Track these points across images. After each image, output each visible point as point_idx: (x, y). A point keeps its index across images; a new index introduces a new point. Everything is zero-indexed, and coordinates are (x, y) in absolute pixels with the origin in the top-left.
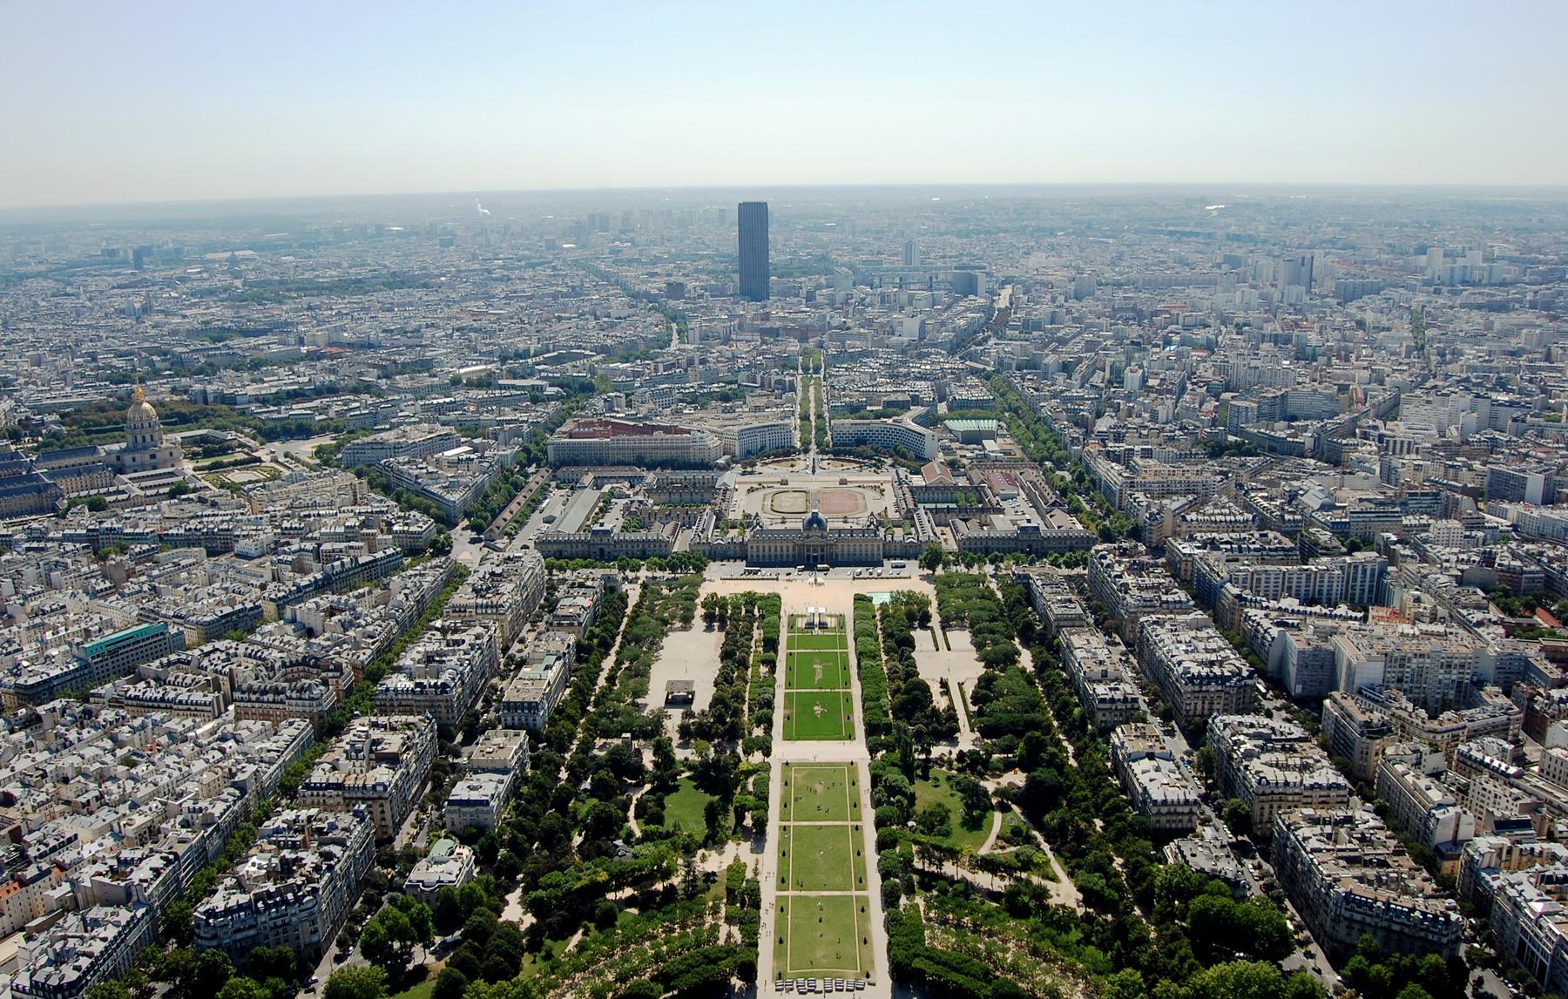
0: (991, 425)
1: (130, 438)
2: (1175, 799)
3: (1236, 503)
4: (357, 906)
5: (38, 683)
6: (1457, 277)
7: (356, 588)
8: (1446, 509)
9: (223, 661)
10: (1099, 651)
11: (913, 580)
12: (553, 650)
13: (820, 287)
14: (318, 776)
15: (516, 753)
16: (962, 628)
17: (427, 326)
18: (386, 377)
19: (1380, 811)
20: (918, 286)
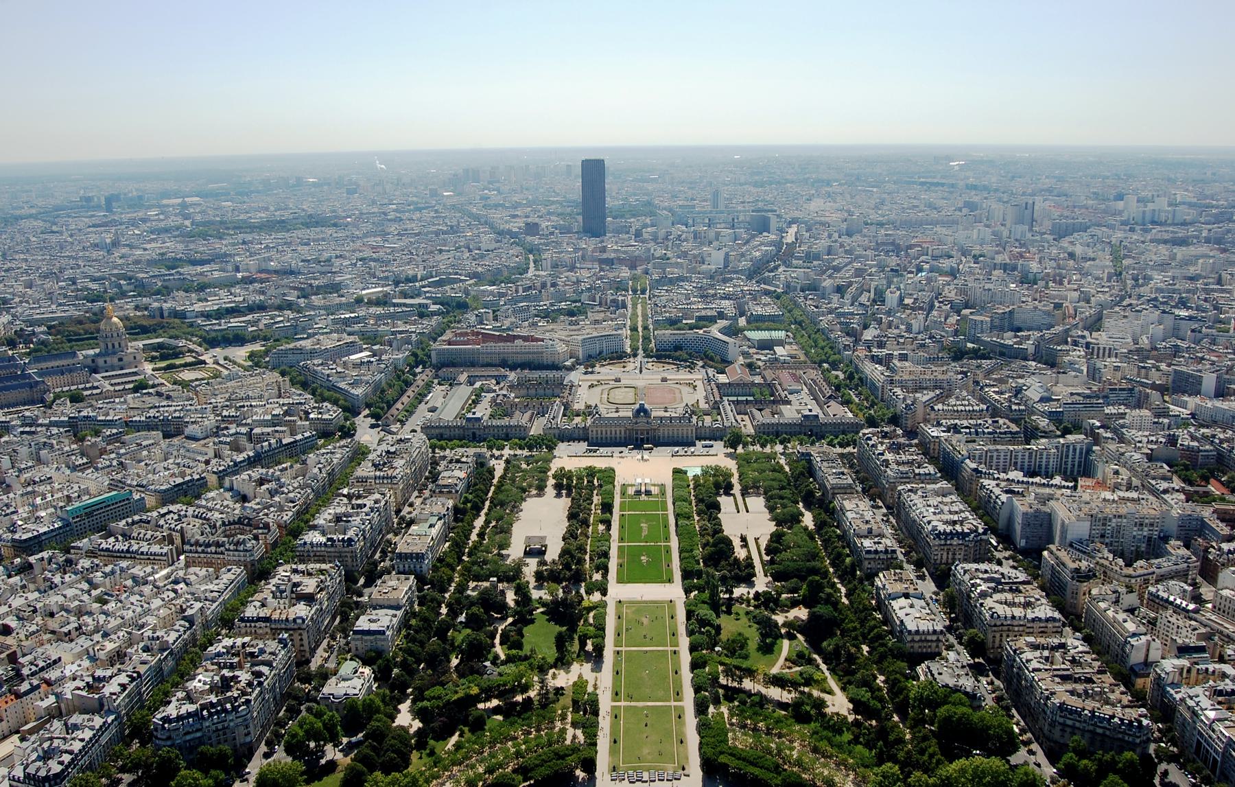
0: (781, 334)
1: (102, 345)
2: (926, 629)
3: (973, 396)
4: (281, 714)
5: (30, 538)
6: (1148, 218)
7: (280, 463)
8: (1139, 401)
9: (176, 521)
10: (865, 513)
11: (719, 457)
12: (435, 512)
13: (646, 226)
14: (250, 612)
15: (406, 593)
16: (758, 495)
17: (337, 257)
18: (304, 297)
19: (1087, 639)
20: (723, 225)
